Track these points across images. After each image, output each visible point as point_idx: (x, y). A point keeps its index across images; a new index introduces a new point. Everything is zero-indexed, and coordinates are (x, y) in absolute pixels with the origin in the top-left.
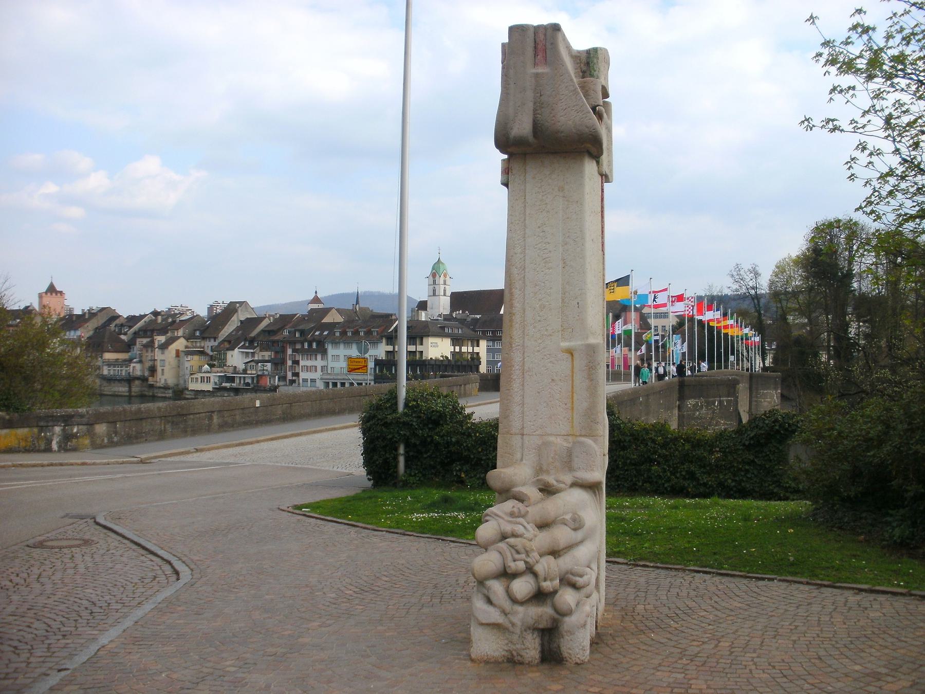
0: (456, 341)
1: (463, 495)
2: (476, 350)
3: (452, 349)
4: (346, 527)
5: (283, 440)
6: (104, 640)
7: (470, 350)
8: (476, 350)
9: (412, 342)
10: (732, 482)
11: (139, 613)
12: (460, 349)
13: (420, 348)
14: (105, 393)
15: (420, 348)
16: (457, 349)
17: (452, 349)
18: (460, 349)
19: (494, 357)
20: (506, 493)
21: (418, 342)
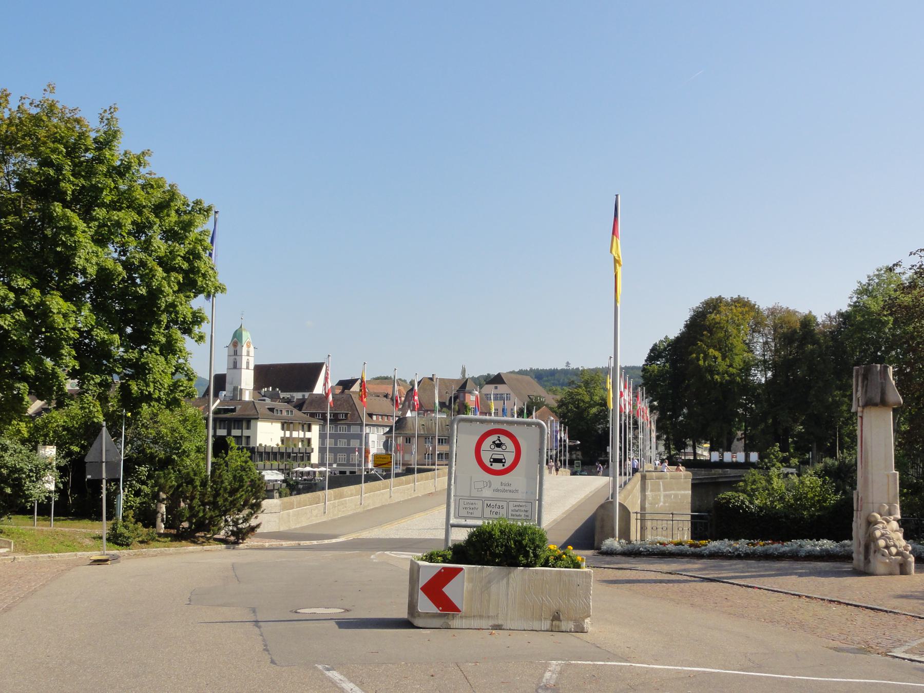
0: (286, 425)
1: (692, 549)
2: (308, 435)
3: (281, 434)
4: (614, 570)
5: (635, 578)
6: (894, 384)
7: (301, 434)
8: (308, 435)
9: (222, 426)
10: (63, 431)
11: (592, 663)
12: (291, 434)
13: (246, 433)
14: (612, 365)
15: (246, 433)
16: (288, 434)
17: (281, 434)
18: (291, 434)
19: (336, 444)
20: (136, 523)
21: (244, 425)
